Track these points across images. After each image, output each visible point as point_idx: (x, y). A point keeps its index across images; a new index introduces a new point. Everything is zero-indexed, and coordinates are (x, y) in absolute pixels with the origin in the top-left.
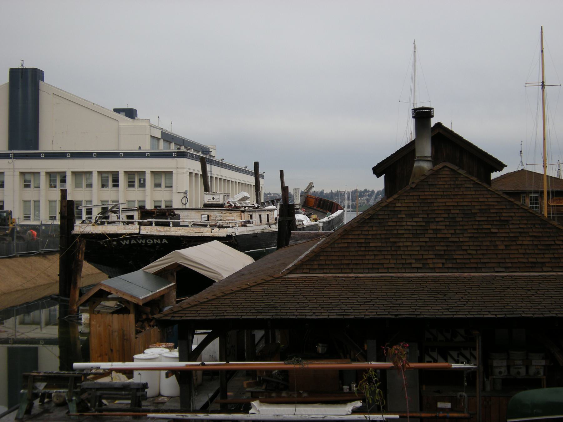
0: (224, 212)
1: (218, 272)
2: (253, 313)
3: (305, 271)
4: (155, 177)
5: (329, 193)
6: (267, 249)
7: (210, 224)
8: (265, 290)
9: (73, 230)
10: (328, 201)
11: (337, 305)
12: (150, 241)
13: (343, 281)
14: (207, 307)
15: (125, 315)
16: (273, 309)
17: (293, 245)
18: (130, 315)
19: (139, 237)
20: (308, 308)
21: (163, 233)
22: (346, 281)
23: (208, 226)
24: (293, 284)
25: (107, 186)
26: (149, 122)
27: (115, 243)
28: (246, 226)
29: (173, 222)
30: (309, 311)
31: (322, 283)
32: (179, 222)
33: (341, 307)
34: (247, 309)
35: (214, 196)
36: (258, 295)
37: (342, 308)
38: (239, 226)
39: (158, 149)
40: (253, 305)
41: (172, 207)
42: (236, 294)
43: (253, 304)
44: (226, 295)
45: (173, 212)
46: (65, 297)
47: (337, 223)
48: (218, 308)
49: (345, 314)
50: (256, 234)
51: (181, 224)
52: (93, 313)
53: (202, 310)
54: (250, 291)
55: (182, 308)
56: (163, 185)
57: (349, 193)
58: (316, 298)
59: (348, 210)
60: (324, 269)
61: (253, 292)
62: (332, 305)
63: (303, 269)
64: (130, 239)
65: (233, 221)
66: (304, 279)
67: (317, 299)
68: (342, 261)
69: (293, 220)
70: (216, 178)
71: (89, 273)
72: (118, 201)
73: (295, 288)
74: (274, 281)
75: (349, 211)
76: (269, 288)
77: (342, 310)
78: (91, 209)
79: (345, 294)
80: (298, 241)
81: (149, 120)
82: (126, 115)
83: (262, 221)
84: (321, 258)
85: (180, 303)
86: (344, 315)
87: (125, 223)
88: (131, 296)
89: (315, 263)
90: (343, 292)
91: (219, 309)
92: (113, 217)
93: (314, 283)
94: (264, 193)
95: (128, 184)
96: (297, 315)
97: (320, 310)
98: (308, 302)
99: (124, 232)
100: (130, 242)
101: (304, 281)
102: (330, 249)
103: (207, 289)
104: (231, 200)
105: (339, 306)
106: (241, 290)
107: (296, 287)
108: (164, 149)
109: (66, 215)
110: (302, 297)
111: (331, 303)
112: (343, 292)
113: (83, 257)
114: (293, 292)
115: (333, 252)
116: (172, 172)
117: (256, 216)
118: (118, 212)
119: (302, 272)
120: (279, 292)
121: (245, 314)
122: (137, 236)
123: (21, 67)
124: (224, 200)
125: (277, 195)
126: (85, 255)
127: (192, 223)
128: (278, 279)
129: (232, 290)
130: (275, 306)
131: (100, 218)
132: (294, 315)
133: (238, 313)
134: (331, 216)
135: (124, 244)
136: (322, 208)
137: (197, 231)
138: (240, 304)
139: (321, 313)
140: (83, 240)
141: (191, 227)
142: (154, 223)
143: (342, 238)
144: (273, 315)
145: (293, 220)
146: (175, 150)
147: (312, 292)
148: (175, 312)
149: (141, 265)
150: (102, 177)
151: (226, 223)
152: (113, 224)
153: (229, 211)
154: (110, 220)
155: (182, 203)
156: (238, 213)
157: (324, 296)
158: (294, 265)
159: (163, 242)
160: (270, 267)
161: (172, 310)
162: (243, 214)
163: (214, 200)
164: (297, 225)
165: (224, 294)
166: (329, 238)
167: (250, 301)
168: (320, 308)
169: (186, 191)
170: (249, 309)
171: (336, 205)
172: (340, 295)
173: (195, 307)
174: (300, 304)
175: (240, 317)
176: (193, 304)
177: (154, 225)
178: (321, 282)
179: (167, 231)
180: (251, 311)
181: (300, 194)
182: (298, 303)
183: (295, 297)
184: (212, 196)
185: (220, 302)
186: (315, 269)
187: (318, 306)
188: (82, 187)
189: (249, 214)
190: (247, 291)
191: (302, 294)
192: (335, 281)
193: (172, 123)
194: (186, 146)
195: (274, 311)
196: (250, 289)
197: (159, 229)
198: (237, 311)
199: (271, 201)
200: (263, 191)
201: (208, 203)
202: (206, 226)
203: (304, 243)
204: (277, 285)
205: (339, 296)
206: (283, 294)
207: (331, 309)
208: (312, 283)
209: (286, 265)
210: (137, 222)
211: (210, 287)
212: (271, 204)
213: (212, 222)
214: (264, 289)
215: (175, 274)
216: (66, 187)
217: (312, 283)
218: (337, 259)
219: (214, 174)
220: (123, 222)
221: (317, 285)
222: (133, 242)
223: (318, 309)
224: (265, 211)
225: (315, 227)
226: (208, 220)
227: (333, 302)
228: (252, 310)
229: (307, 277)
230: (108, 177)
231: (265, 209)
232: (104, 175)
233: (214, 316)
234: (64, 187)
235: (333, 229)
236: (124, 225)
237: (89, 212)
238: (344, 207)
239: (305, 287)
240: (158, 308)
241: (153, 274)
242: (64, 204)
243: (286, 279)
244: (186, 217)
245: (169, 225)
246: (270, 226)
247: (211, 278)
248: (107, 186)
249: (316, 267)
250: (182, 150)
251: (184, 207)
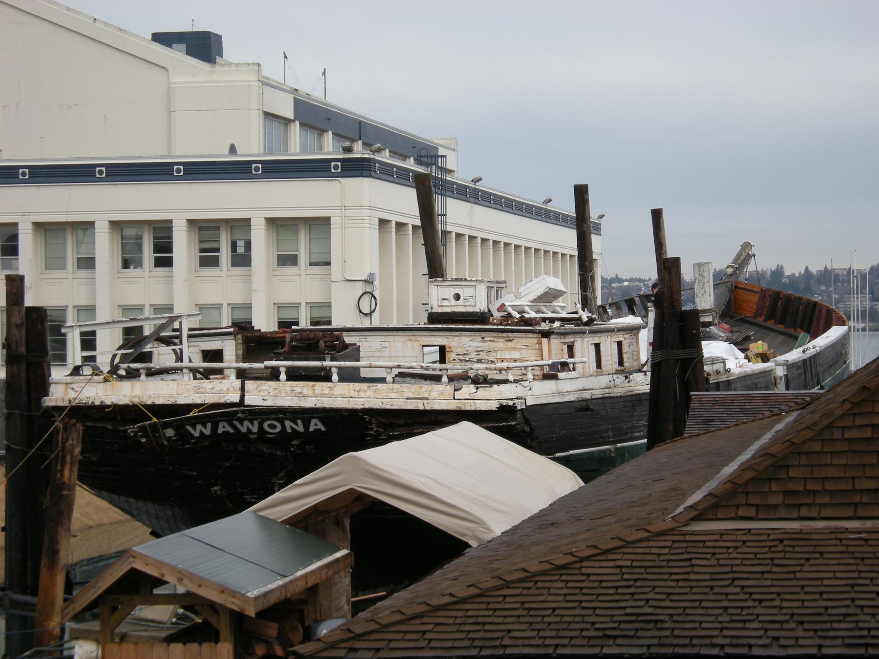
0: (489, 336)
1: (480, 520)
2: (590, 638)
3: (742, 512)
4: (45, 235)
5: (800, 276)
6: (619, 445)
7: (450, 372)
8: (624, 570)
9: (47, 395)
10: (800, 299)
11: (845, 615)
12: (273, 427)
13: (862, 542)
14: (451, 621)
15: (206, 646)
16: (651, 626)
17: (699, 435)
18: (219, 645)
19: (240, 415)
20: (755, 625)
21: (310, 403)
22: (870, 543)
23: (445, 379)
24: (705, 550)
25: (139, 264)
26: (259, 71)
27: (170, 432)
28: (554, 377)
29: (340, 368)
30: (761, 633)
31: (797, 549)
32: (358, 369)
33: (857, 622)
34: (572, 626)
36: (604, 584)
37: (861, 625)
38: (534, 379)
39: (286, 151)
40: (589, 615)
41: (329, 323)
42: (537, 582)
43: (590, 612)
44: (507, 585)
45: (338, 338)
46: (25, 593)
47: (830, 366)
48: (484, 624)
49: (870, 641)
50: (586, 400)
51: (362, 375)
52: (113, 641)
53: (438, 628)
54: (577, 571)
55: (378, 623)
56: (303, 259)
57: (863, 276)
58: (779, 594)
59: (861, 325)
60: (803, 505)
61: (589, 575)
62: (830, 615)
63: (738, 506)
64: (214, 420)
65: (518, 364)
66: (740, 538)
67: (782, 596)
68: (857, 481)
69: (694, 358)
70: (459, 236)
71: (91, 523)
72: (170, 308)
73: (714, 562)
74: (652, 544)
75: (864, 330)
76: (635, 564)
77: (861, 629)
78: (94, 333)
79: (868, 582)
80: (712, 421)
81: (259, 65)
82: (189, 53)
83: (603, 363)
84: (792, 474)
85: (372, 608)
86: (867, 646)
87: (200, 372)
88: (223, 590)
89: (774, 487)
90: (862, 575)
91: (487, 627)
92: (163, 356)
93: (773, 549)
94: (602, 278)
95: (200, 257)
96: (722, 646)
97: (793, 630)
98: (754, 607)
99: (197, 399)
100: (215, 428)
101: (740, 544)
102: (817, 447)
103: (448, 567)
104: (509, 300)
105: (850, 619)
106: (550, 570)
107: (719, 560)
108: (304, 149)
109: (23, 350)
110: (738, 590)
111: (826, 608)
112: (862, 575)
113: (75, 475)
114: (708, 577)
115: (829, 456)
116: (328, 219)
117: (584, 347)
118: (177, 341)
119: (733, 515)
120: (667, 577)
121: (566, 642)
122: (236, 412)
124: (489, 302)
125: (642, 285)
126: (79, 470)
127: (396, 371)
128: (662, 538)
129: (526, 571)
130: (654, 618)
131: (124, 358)
132: (714, 645)
133: (545, 638)
134: (810, 345)
135: (196, 434)
136: (782, 321)
137: (411, 396)
138: (549, 612)
139: (797, 638)
140: (74, 425)
141: (393, 382)
142: (283, 371)
143: (856, 411)
144: (649, 646)
145: (694, 358)
146: (338, 153)
147: (766, 576)
148: (358, 637)
149: (248, 497)
150: (122, 239)
151: (495, 369)
152: (164, 376)
153: (505, 335)
154: (155, 364)
155: (360, 311)
156: (532, 340)
157: (803, 587)
158: (710, 494)
159: (312, 429)
160: (634, 502)
161: (349, 630)
162: (545, 341)
163: (461, 302)
164: (709, 374)
165: (502, 582)
166: (814, 412)
167: (581, 602)
168: (793, 625)
169: (372, 275)
170: (577, 626)
171: (824, 312)
172: (853, 586)
173: (418, 621)
174: (730, 611)
175: (550, 651)
176: (410, 612)
177: (283, 376)
178: (794, 547)
179: (323, 395)
180: (585, 633)
181: (714, 280)
182: (726, 608)
183: (716, 590)
184: (454, 291)
185: (491, 606)
186: (775, 507)
187: (787, 618)
188: (64, 267)
189: (564, 343)
190: (569, 571)
191: (736, 583)
192: (838, 542)
193: (324, 73)
194: (369, 142)
195: (655, 633)
196: (578, 565)
197: (298, 390)
198: (541, 634)
199: (626, 301)
200: (601, 272)
201: (440, 310)
202: (437, 379)
203: (732, 429)
204: (659, 555)
205: (849, 589)
206: (678, 581)
207: (828, 626)
208: (766, 550)
209: (685, 495)
210: (235, 368)
211: (456, 561)
212: (625, 309)
213: (454, 367)
214: (621, 567)
215: (347, 523)
216: (17, 268)
217: (766, 550)
218: (842, 475)
219: (454, 224)
220: (194, 371)
221: (782, 555)
222: (223, 427)
223: (785, 626)
224: (611, 331)
225: (764, 379)
226: (442, 360)
227: (833, 607)
228: (588, 629)
229: (750, 530)
230: (140, 238)
231: (613, 326)
232: (130, 232)
233: (475, 647)
234: (11, 268)
235: (818, 383)
236: (195, 378)
237: (89, 342)
238: (849, 318)
239: (744, 562)
240: (299, 625)
241: (285, 522)
242: (16, 319)
243: (688, 538)
244: (378, 354)
245: (327, 378)
246: (626, 377)
247: (456, 533)
248: (139, 264)
249: (776, 500)
250: (358, 152)
251: (366, 324)
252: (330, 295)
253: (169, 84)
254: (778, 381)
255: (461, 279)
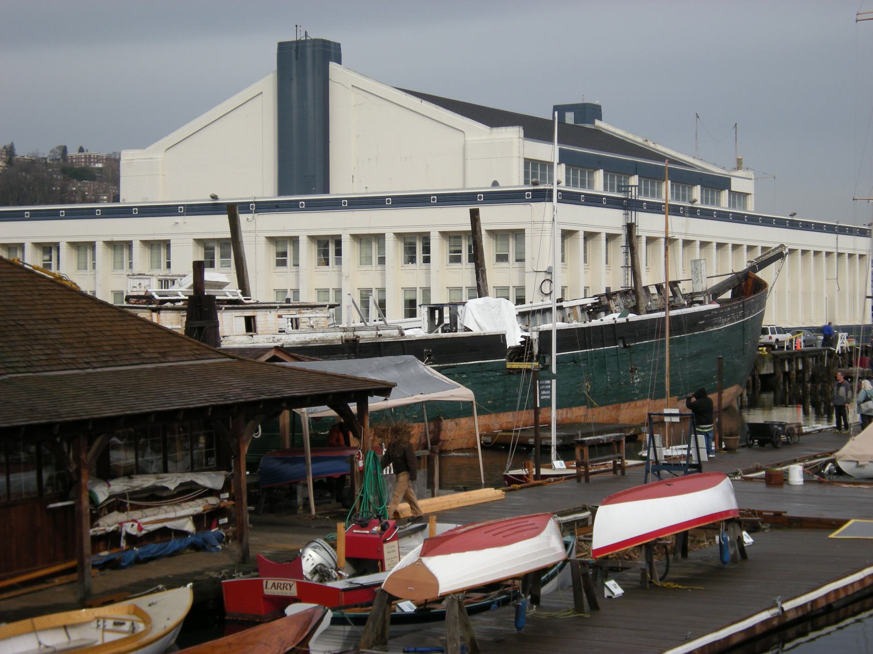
35: (141, 281)
95: (424, 257)
123: (304, 39)
219: (644, 231)
252: (525, 281)
253: (465, 141)
254: (534, 342)
255: (144, 274)
